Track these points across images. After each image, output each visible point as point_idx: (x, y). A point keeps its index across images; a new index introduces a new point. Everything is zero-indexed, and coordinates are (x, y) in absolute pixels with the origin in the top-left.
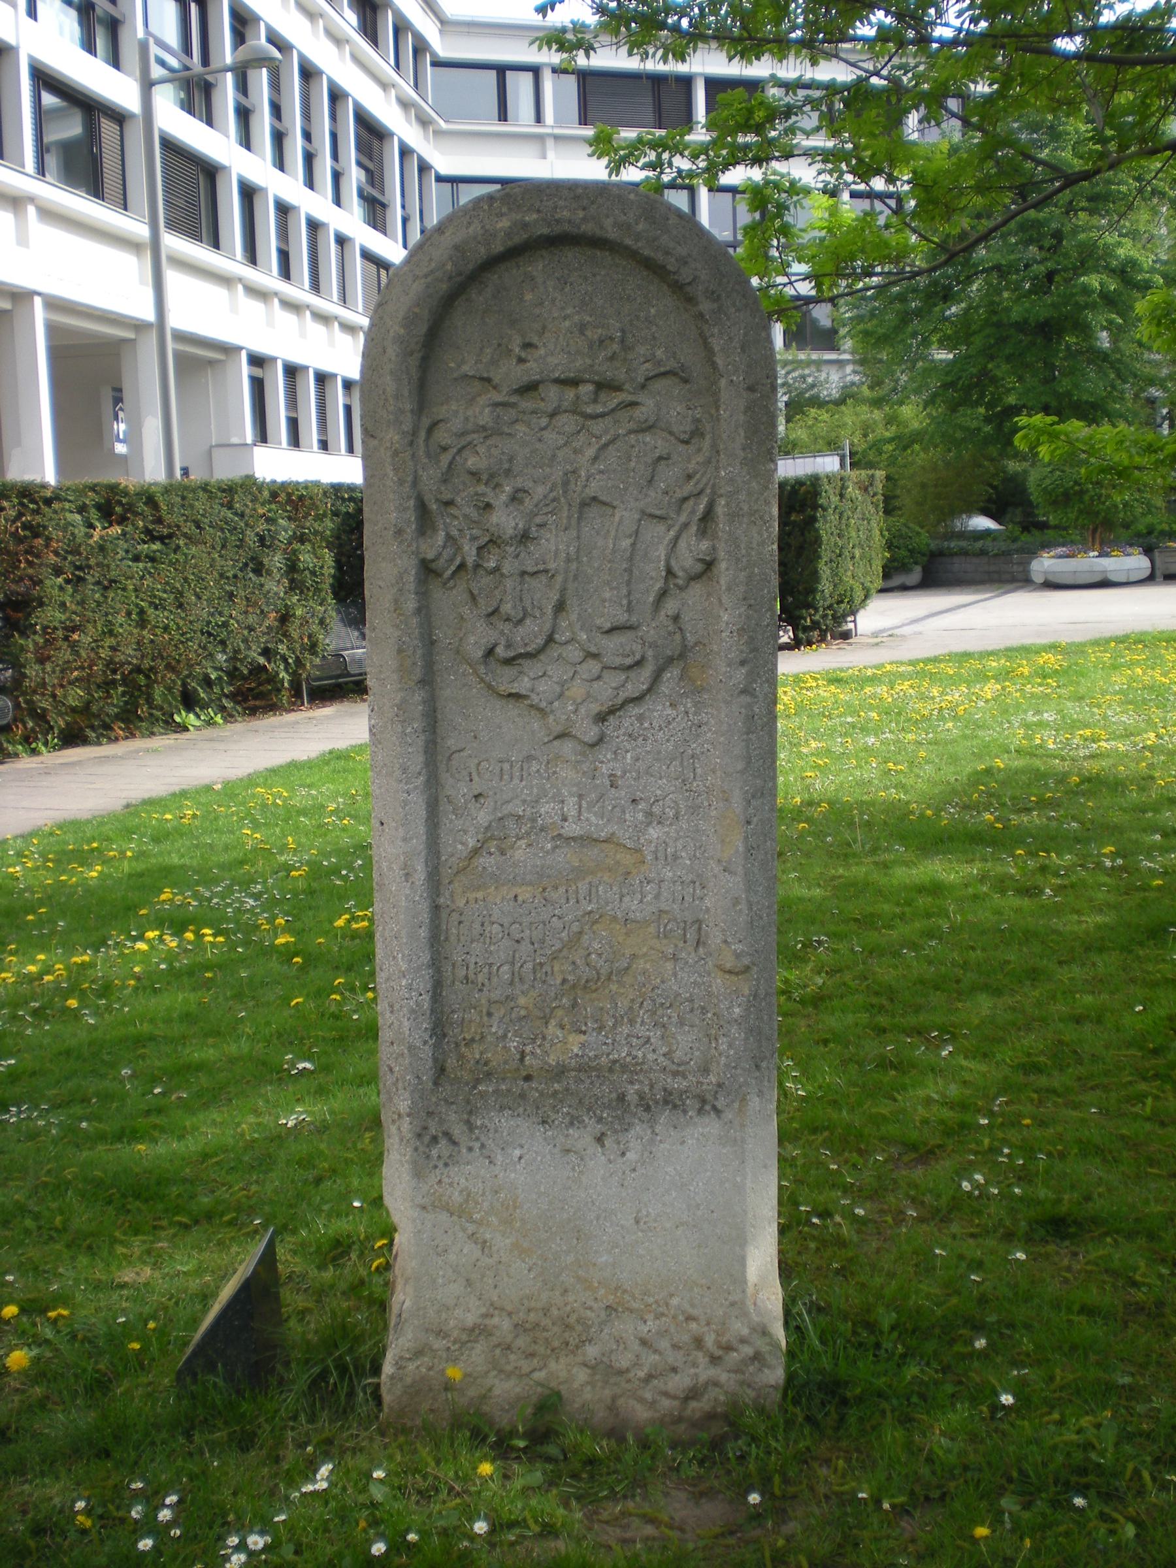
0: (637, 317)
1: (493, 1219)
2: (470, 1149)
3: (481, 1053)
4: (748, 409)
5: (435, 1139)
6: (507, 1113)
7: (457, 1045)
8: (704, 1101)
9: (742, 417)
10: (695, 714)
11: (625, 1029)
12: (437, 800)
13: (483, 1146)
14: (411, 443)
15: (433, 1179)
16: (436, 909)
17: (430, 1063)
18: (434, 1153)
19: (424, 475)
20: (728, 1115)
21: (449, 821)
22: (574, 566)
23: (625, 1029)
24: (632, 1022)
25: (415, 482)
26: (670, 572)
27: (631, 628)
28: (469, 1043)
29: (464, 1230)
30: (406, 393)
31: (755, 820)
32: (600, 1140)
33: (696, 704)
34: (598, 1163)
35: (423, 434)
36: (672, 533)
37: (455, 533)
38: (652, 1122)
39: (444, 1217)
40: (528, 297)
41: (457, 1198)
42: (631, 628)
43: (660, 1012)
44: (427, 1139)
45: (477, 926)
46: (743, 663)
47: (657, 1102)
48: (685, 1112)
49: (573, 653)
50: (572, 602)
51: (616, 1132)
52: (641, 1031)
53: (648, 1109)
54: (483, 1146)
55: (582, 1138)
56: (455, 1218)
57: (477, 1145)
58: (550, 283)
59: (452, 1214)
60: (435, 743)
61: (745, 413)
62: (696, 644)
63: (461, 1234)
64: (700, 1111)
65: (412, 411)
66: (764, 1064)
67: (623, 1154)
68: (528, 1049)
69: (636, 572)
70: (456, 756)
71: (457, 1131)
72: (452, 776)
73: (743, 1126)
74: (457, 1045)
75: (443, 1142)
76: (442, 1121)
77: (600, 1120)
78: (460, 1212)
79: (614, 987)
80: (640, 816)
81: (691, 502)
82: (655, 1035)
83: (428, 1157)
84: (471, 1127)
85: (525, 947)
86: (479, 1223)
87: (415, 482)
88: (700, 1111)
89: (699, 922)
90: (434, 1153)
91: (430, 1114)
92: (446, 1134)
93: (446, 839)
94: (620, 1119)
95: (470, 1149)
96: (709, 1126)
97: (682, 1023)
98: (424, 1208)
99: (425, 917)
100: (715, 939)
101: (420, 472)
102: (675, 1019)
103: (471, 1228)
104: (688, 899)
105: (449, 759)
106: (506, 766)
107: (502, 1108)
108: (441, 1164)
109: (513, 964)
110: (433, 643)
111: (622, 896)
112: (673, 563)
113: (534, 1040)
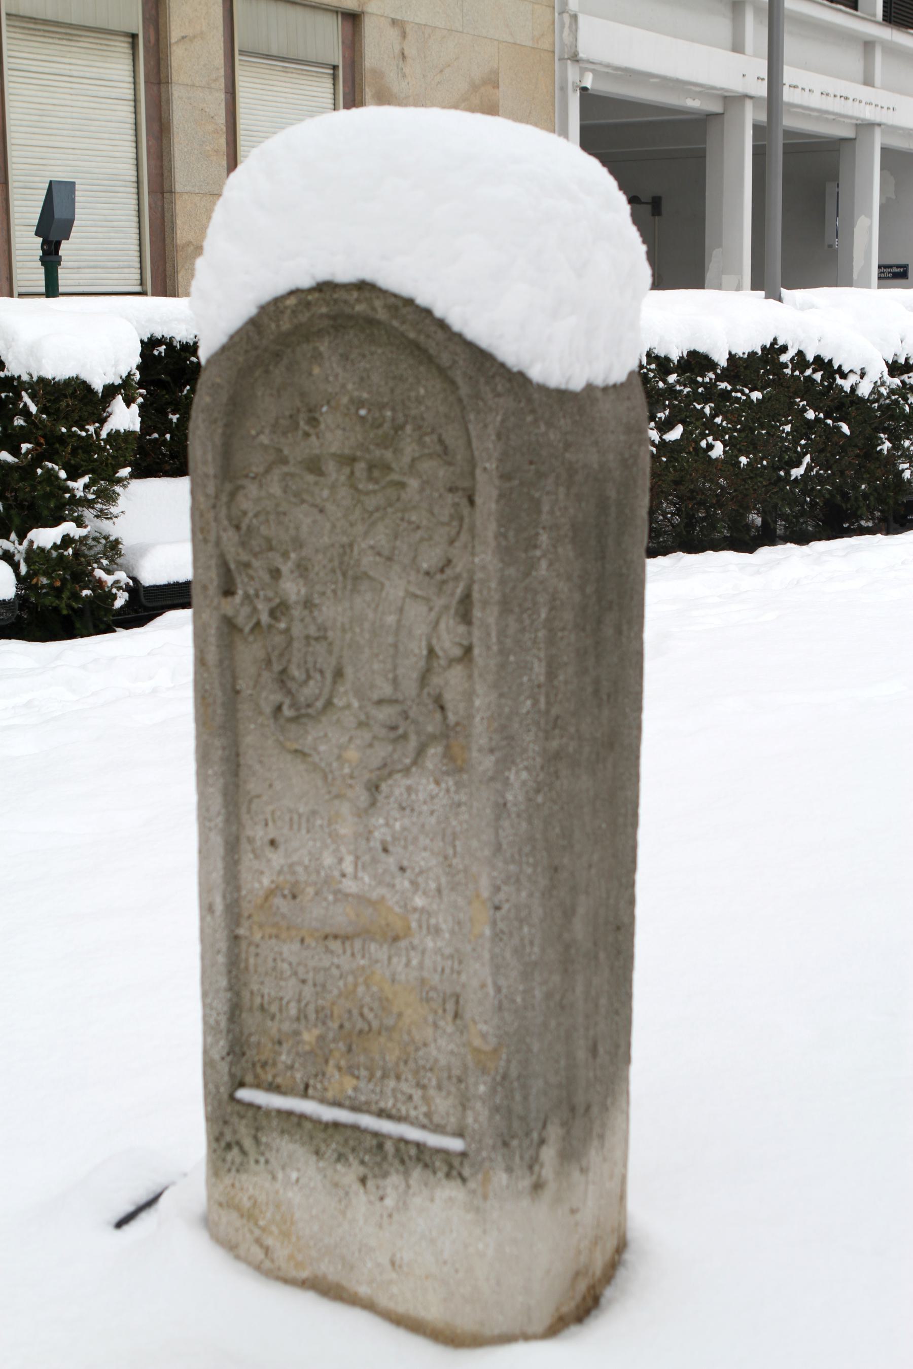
0: (409, 398)
1: (274, 1229)
2: (257, 1162)
3: (274, 1076)
4: (501, 496)
5: (229, 1146)
6: (286, 1137)
7: (254, 1065)
8: (451, 1167)
9: (493, 506)
10: (456, 792)
11: (392, 1083)
12: (237, 839)
13: (267, 1162)
14: (214, 507)
15: (228, 1180)
16: (235, 939)
17: (226, 1078)
18: (229, 1157)
19: (225, 536)
20: (472, 1185)
21: (247, 860)
22: (348, 636)
23: (392, 1083)
24: (398, 1078)
25: (218, 543)
26: (431, 651)
27: (396, 701)
28: (264, 1065)
29: (252, 1232)
30: (210, 457)
31: (506, 906)
32: (363, 1181)
33: (456, 784)
34: (361, 1200)
35: (224, 498)
36: (433, 614)
37: (252, 592)
38: (407, 1174)
39: (234, 1215)
40: (316, 370)
41: (246, 1204)
42: (396, 701)
43: (422, 1073)
44: (223, 1144)
45: (270, 960)
46: (492, 751)
47: (410, 1158)
48: (435, 1173)
49: (349, 720)
50: (349, 671)
51: (375, 1176)
52: (405, 1087)
53: (403, 1162)
54: (267, 1162)
55: (349, 1174)
56: (245, 1221)
57: (262, 1160)
58: (333, 359)
59: (242, 1216)
60: (237, 786)
61: (497, 502)
62: (457, 724)
63: (248, 1235)
64: (448, 1175)
65: (215, 476)
66: (515, 1143)
67: (382, 1199)
68: (312, 1082)
69: (401, 648)
70: (256, 801)
71: (248, 1143)
72: (252, 818)
73: (485, 1197)
74: (254, 1065)
75: (235, 1150)
76: (235, 1132)
77: (362, 1162)
78: (249, 1215)
79: (382, 1040)
80: (407, 884)
81: (451, 584)
82: (417, 1094)
83: (224, 1160)
84: (256, 1139)
85: (308, 991)
86: (263, 1229)
87: (218, 543)
88: (448, 1175)
89: (457, 997)
90: (229, 1157)
91: (226, 1122)
92: (239, 1144)
93: (246, 876)
94: (379, 1165)
95: (257, 1162)
96: (451, 1191)
97: (439, 1087)
98: (221, 1205)
99: (223, 945)
100: (471, 1010)
101: (222, 533)
102: (434, 1082)
103: (257, 1232)
104: (447, 971)
105: (250, 802)
106: (296, 817)
107: (283, 1132)
108: (234, 1170)
109: (299, 1001)
110: (238, 692)
111: (390, 959)
112: (434, 642)
113: (316, 1076)
